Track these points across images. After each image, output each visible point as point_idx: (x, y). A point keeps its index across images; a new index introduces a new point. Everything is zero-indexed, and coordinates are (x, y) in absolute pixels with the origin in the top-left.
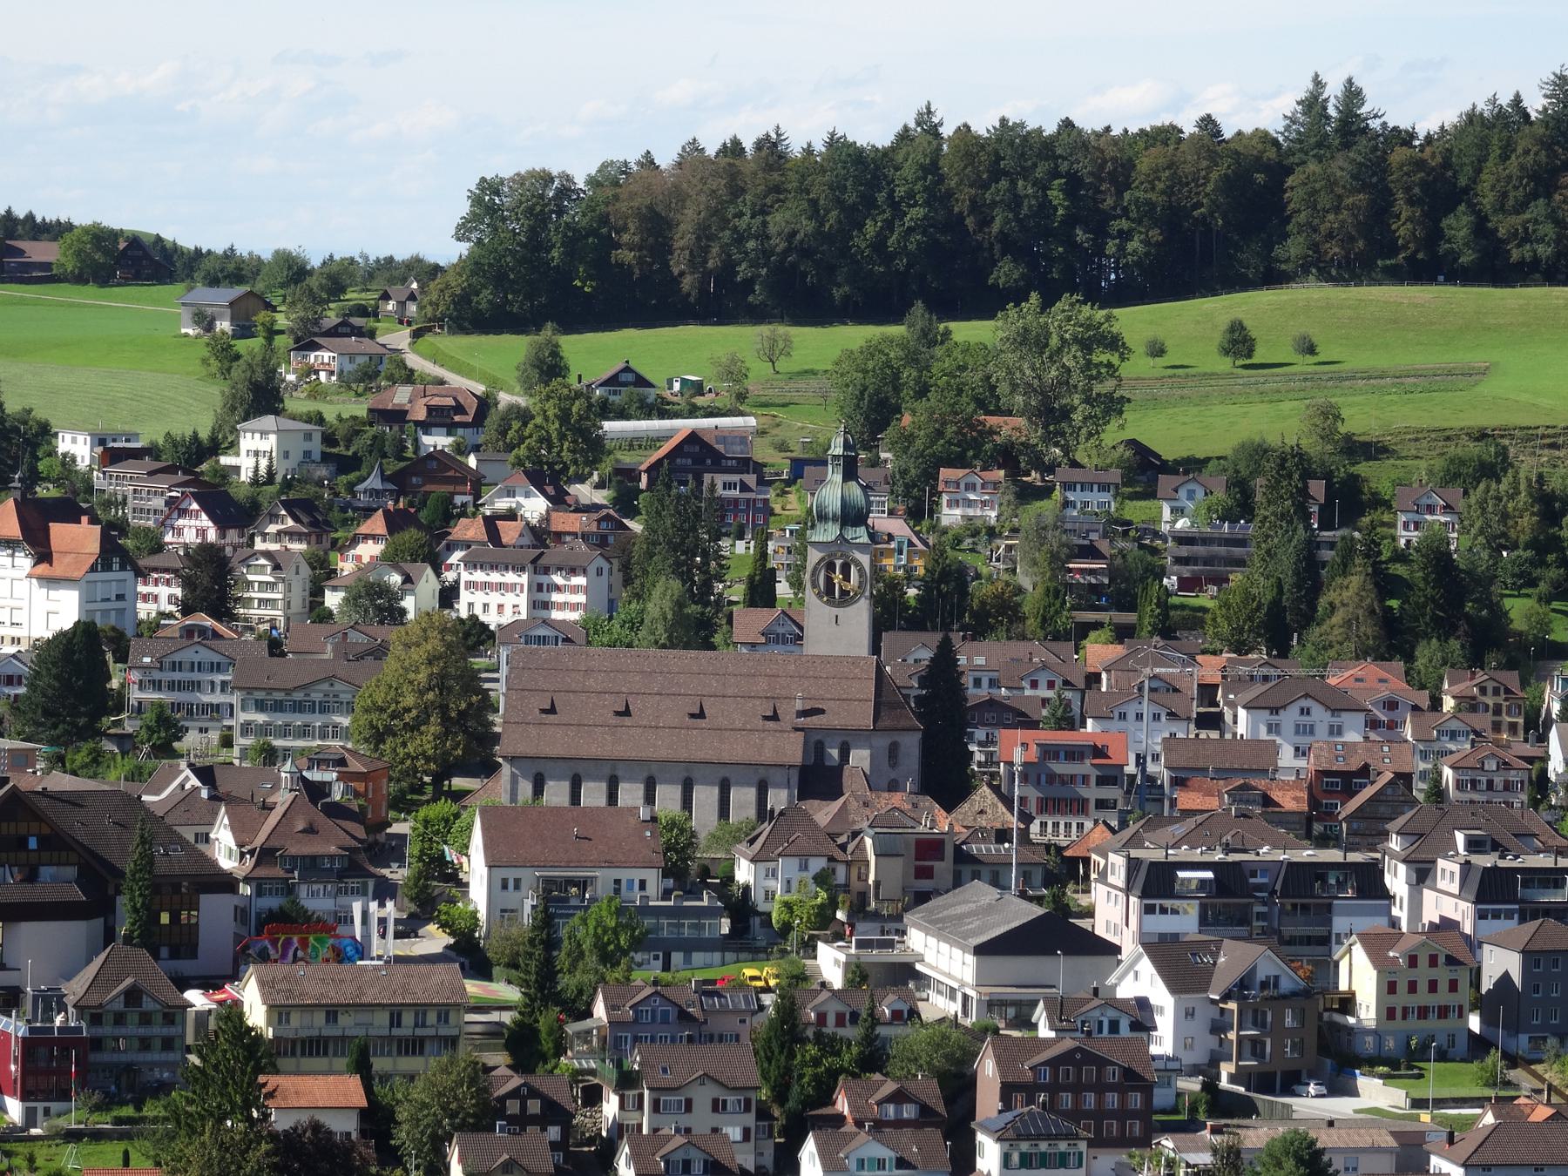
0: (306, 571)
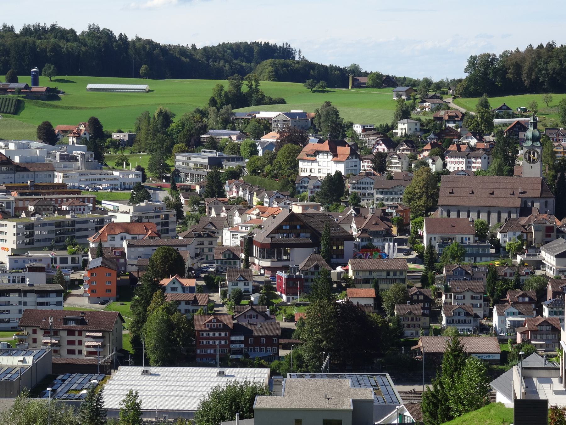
0: (407, 159)
